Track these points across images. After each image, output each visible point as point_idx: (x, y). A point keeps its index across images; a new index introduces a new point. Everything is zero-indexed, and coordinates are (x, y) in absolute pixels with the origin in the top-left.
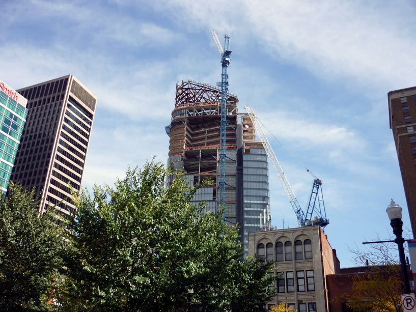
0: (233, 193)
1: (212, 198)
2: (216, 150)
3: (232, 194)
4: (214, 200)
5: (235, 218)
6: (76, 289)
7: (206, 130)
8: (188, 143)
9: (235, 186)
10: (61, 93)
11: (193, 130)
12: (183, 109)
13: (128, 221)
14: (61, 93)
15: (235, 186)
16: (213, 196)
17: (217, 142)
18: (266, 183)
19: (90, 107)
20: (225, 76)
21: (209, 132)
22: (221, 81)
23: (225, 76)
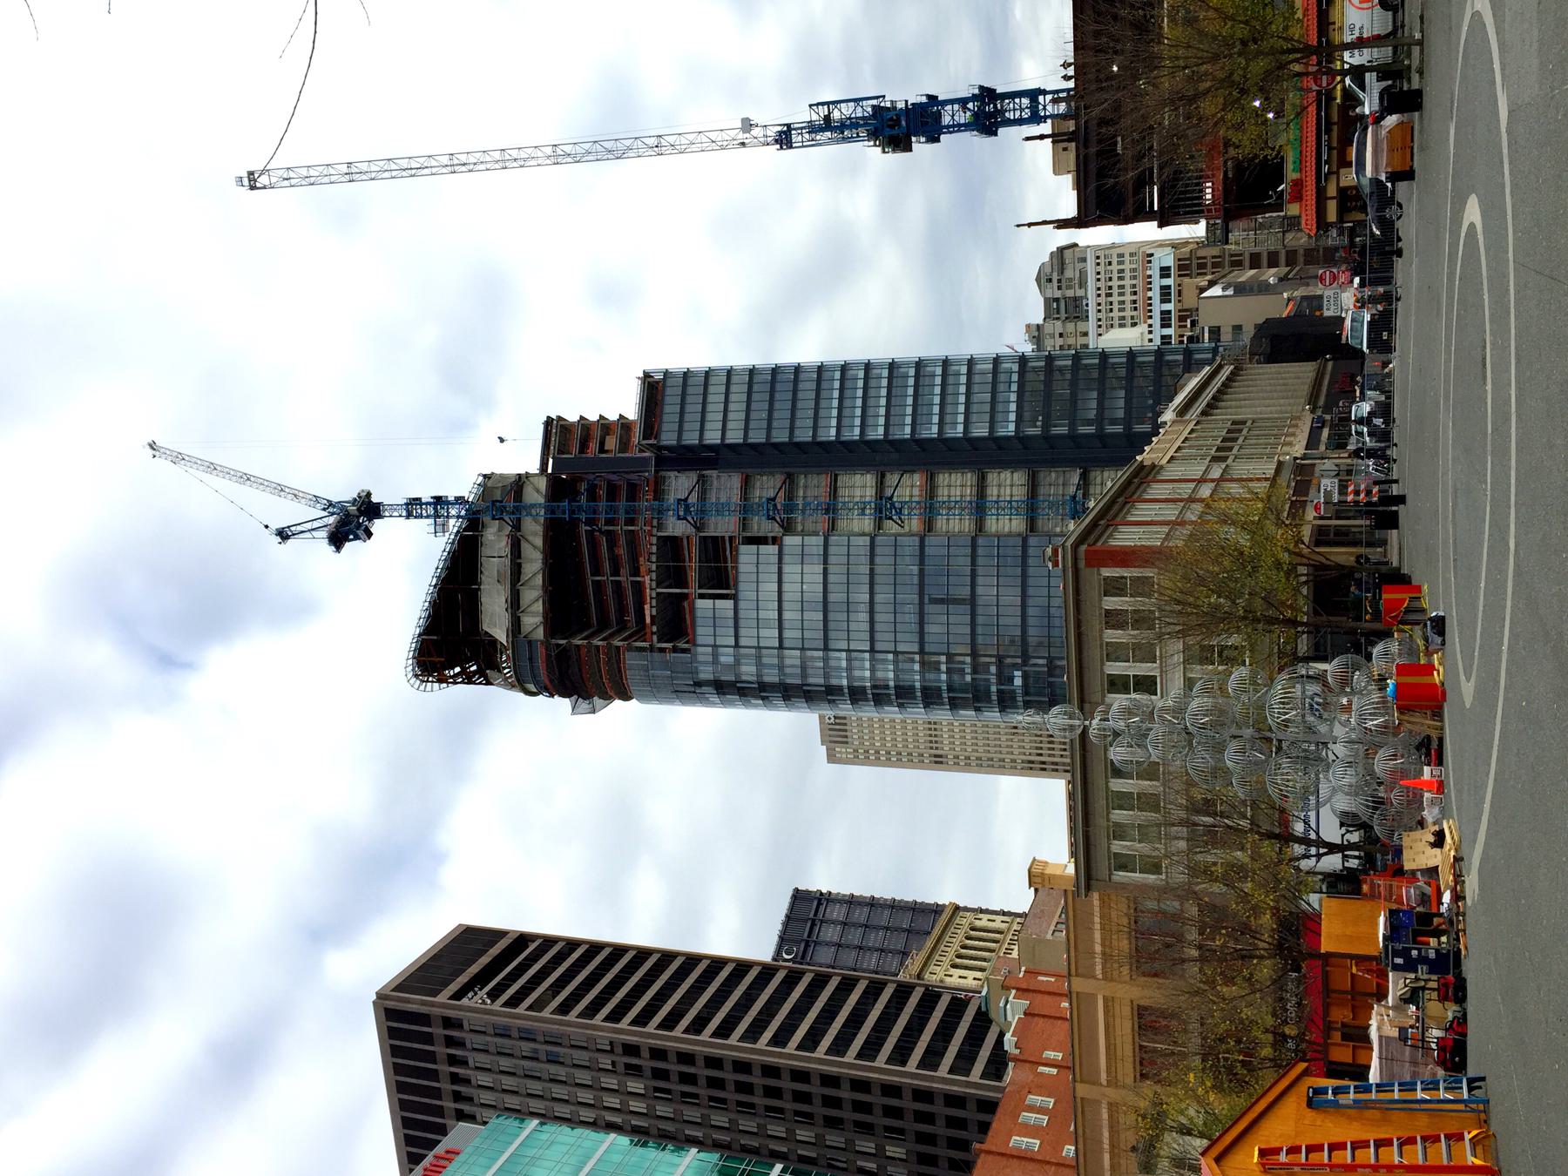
0: (802, 482)
1: (773, 549)
2: (659, 538)
3: (806, 487)
4: (775, 540)
5: (883, 476)
6: (981, 838)
7: (590, 579)
8: (630, 636)
9: (779, 478)
10: (438, 1031)
11: (589, 626)
12: (598, 662)
13: (1380, 784)
14: (438, 1031)
15: (694, 476)
16: (766, 543)
17: (633, 540)
18: (708, 373)
19: (492, 944)
20: (412, 507)
21: (597, 570)
22: (431, 521)
23: (412, 507)
